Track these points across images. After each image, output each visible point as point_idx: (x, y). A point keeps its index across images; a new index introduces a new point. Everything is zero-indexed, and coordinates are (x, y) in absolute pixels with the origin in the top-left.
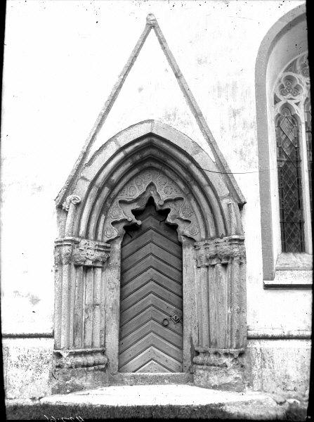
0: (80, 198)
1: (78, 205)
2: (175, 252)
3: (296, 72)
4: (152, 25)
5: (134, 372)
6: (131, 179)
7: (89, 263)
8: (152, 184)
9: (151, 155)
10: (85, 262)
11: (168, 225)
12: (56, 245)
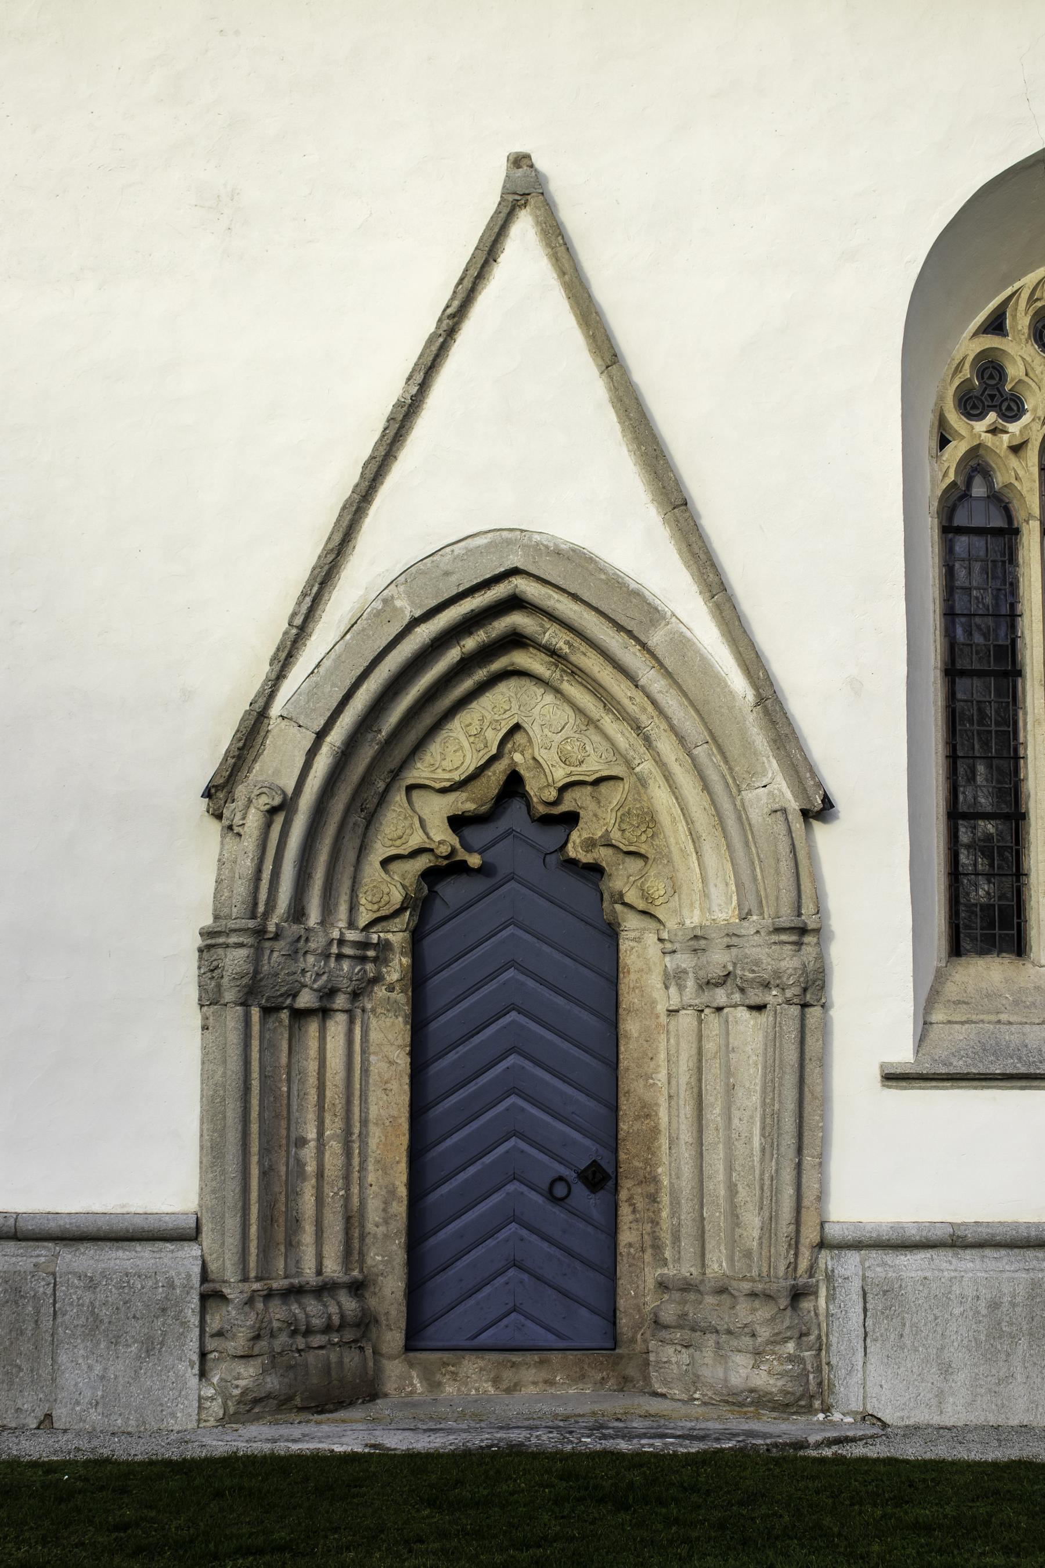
4: (526, 189)
7: (306, 999)
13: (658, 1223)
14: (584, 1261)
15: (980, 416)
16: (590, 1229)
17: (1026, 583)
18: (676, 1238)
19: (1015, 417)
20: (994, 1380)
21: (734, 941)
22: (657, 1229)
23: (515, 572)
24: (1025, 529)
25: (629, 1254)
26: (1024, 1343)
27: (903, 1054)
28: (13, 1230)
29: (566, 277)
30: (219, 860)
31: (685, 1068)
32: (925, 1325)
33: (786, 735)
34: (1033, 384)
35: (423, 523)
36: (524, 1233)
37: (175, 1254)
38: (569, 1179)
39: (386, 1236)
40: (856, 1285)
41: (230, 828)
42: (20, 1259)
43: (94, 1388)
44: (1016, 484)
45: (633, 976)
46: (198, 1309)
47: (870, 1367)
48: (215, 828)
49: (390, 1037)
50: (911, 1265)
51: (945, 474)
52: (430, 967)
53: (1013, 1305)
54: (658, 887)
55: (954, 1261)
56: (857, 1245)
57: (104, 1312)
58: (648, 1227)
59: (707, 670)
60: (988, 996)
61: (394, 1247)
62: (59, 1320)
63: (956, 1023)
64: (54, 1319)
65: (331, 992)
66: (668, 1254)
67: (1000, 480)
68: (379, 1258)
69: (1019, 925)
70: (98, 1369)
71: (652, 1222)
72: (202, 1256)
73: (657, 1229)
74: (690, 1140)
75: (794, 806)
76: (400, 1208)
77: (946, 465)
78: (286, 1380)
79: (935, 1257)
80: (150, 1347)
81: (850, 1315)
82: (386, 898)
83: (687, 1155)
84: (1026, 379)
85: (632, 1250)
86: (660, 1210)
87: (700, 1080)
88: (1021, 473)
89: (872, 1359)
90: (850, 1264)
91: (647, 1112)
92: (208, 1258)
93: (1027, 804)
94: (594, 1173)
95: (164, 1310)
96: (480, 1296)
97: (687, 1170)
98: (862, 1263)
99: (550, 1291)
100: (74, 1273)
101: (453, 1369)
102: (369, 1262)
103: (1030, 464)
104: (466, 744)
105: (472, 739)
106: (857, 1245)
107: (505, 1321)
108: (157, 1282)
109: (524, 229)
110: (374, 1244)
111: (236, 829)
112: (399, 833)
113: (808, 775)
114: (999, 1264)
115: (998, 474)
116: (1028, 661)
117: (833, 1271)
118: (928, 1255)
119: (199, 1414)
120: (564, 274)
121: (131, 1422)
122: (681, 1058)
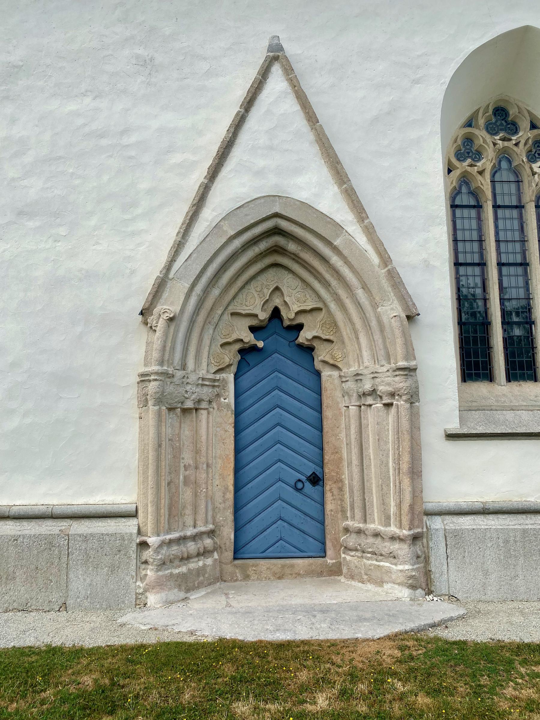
0: (175, 308)
1: (171, 320)
2: (314, 514)
3: (477, 127)
4: (276, 56)
5: (263, 552)
6: (253, 278)
7: (189, 404)
8: (277, 289)
9: (276, 241)
10: (182, 403)
11: (300, 346)
12: (138, 380)
13: (343, 501)
14: (312, 518)
15: (464, 160)
16: (313, 502)
17: (487, 227)
18: (352, 508)
19: (479, 160)
20: (509, 578)
21: (376, 375)
22: (343, 503)
23: (276, 215)
24: (485, 205)
25: (331, 514)
26: (521, 560)
27: (454, 425)
28: (51, 514)
29: (296, 88)
30: (146, 342)
31: (354, 431)
32: (475, 551)
33: (399, 282)
34: (486, 146)
35: (236, 189)
36: (285, 505)
37: (126, 524)
38: (304, 481)
39: (224, 508)
40: (441, 534)
41: (151, 327)
42: (53, 527)
43: (86, 590)
44: (481, 186)
45: (328, 392)
46: (136, 551)
47: (450, 572)
48: (144, 330)
49: (225, 420)
50: (466, 522)
51: (452, 183)
52: (242, 408)
53: (516, 542)
54: (339, 354)
55: (485, 520)
56: (440, 513)
57: (92, 553)
58: (339, 502)
59: (362, 253)
60: (484, 398)
61: (228, 513)
62: (70, 557)
63: (473, 410)
64: (68, 557)
65: (199, 401)
66: (349, 514)
67: (473, 186)
68: (221, 519)
69: (490, 369)
70: (88, 580)
71: (341, 500)
72: (138, 524)
73: (343, 503)
74: (358, 464)
75: (403, 315)
76: (230, 496)
77: (452, 179)
78: (177, 583)
79: (476, 518)
80: (113, 569)
81: (439, 547)
82: (222, 361)
83: (356, 470)
84: (483, 144)
85: (332, 513)
86: (344, 495)
87: (361, 437)
88: (483, 182)
89: (451, 569)
90: (437, 523)
91: (337, 451)
92: (141, 525)
93: (491, 318)
94: (314, 477)
95: (119, 551)
96: (265, 533)
97: (356, 476)
98: (443, 522)
99: (296, 530)
100: (78, 535)
101: (254, 569)
102: (217, 520)
103: (486, 178)
104: (256, 295)
105: (258, 293)
106: (440, 513)
107: (277, 544)
108: (116, 538)
109: (276, 70)
110: (219, 512)
111: (154, 328)
112: (228, 333)
113: (409, 300)
114: (506, 522)
115: (473, 183)
116: (489, 259)
117: (430, 526)
118: (472, 518)
119: (136, 601)
120: (295, 86)
121: (103, 606)
122: (351, 427)
